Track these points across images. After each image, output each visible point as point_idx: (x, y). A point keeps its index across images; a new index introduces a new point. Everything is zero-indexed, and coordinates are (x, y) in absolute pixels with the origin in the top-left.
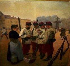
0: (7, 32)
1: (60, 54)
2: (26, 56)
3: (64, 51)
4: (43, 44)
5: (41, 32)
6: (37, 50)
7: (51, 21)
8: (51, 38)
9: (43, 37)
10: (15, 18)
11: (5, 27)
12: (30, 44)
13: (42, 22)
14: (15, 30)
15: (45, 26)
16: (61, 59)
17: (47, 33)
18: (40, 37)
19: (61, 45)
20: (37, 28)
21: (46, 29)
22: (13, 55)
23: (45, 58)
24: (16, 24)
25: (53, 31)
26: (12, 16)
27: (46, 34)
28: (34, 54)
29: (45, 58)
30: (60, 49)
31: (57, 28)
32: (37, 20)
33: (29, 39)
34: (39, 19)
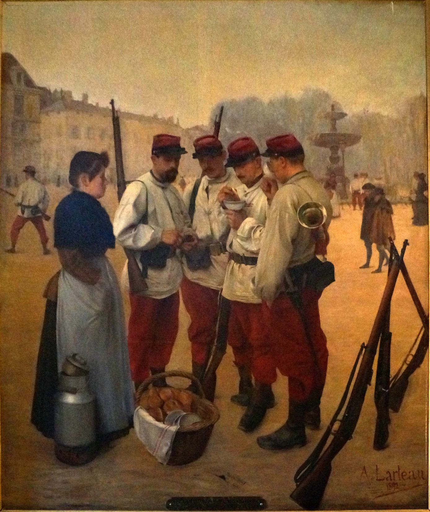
0: (44, 199)
1: (370, 392)
2: (151, 391)
3: (397, 365)
4: (256, 300)
5: (243, 213)
6: (222, 350)
7: (295, 130)
8: (304, 258)
9: (254, 249)
10: (95, 109)
11: (39, 166)
12: (177, 295)
13: (246, 134)
14: (90, 187)
15: (260, 167)
16: (381, 441)
17: (273, 215)
18: (237, 243)
19: (371, 313)
20: (216, 178)
21: (270, 188)
22: (72, 382)
23: (276, 420)
24: (99, 151)
25: (317, 206)
26: (77, 97)
27: (272, 225)
28: (203, 383)
29: (276, 420)
30: (369, 350)
31: (334, 181)
32: (217, 125)
33: (170, 263)
34: (228, 114)
